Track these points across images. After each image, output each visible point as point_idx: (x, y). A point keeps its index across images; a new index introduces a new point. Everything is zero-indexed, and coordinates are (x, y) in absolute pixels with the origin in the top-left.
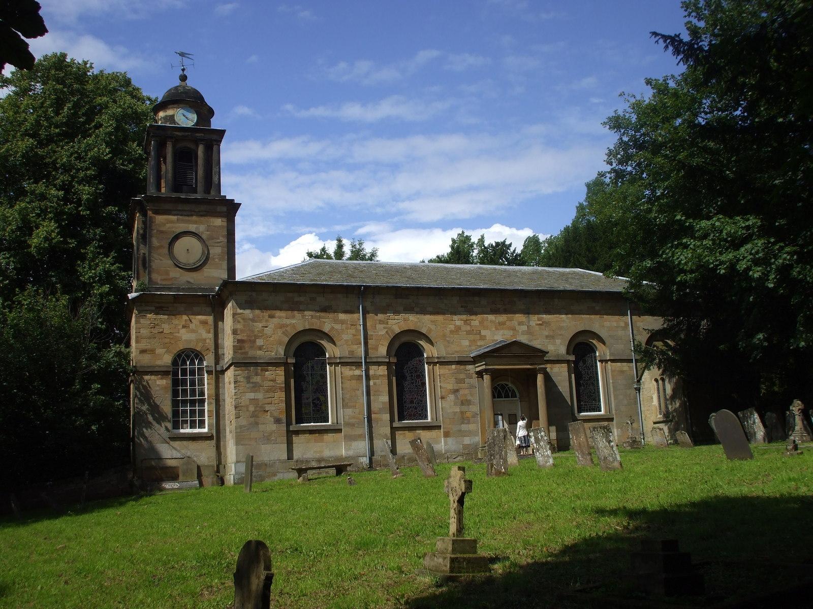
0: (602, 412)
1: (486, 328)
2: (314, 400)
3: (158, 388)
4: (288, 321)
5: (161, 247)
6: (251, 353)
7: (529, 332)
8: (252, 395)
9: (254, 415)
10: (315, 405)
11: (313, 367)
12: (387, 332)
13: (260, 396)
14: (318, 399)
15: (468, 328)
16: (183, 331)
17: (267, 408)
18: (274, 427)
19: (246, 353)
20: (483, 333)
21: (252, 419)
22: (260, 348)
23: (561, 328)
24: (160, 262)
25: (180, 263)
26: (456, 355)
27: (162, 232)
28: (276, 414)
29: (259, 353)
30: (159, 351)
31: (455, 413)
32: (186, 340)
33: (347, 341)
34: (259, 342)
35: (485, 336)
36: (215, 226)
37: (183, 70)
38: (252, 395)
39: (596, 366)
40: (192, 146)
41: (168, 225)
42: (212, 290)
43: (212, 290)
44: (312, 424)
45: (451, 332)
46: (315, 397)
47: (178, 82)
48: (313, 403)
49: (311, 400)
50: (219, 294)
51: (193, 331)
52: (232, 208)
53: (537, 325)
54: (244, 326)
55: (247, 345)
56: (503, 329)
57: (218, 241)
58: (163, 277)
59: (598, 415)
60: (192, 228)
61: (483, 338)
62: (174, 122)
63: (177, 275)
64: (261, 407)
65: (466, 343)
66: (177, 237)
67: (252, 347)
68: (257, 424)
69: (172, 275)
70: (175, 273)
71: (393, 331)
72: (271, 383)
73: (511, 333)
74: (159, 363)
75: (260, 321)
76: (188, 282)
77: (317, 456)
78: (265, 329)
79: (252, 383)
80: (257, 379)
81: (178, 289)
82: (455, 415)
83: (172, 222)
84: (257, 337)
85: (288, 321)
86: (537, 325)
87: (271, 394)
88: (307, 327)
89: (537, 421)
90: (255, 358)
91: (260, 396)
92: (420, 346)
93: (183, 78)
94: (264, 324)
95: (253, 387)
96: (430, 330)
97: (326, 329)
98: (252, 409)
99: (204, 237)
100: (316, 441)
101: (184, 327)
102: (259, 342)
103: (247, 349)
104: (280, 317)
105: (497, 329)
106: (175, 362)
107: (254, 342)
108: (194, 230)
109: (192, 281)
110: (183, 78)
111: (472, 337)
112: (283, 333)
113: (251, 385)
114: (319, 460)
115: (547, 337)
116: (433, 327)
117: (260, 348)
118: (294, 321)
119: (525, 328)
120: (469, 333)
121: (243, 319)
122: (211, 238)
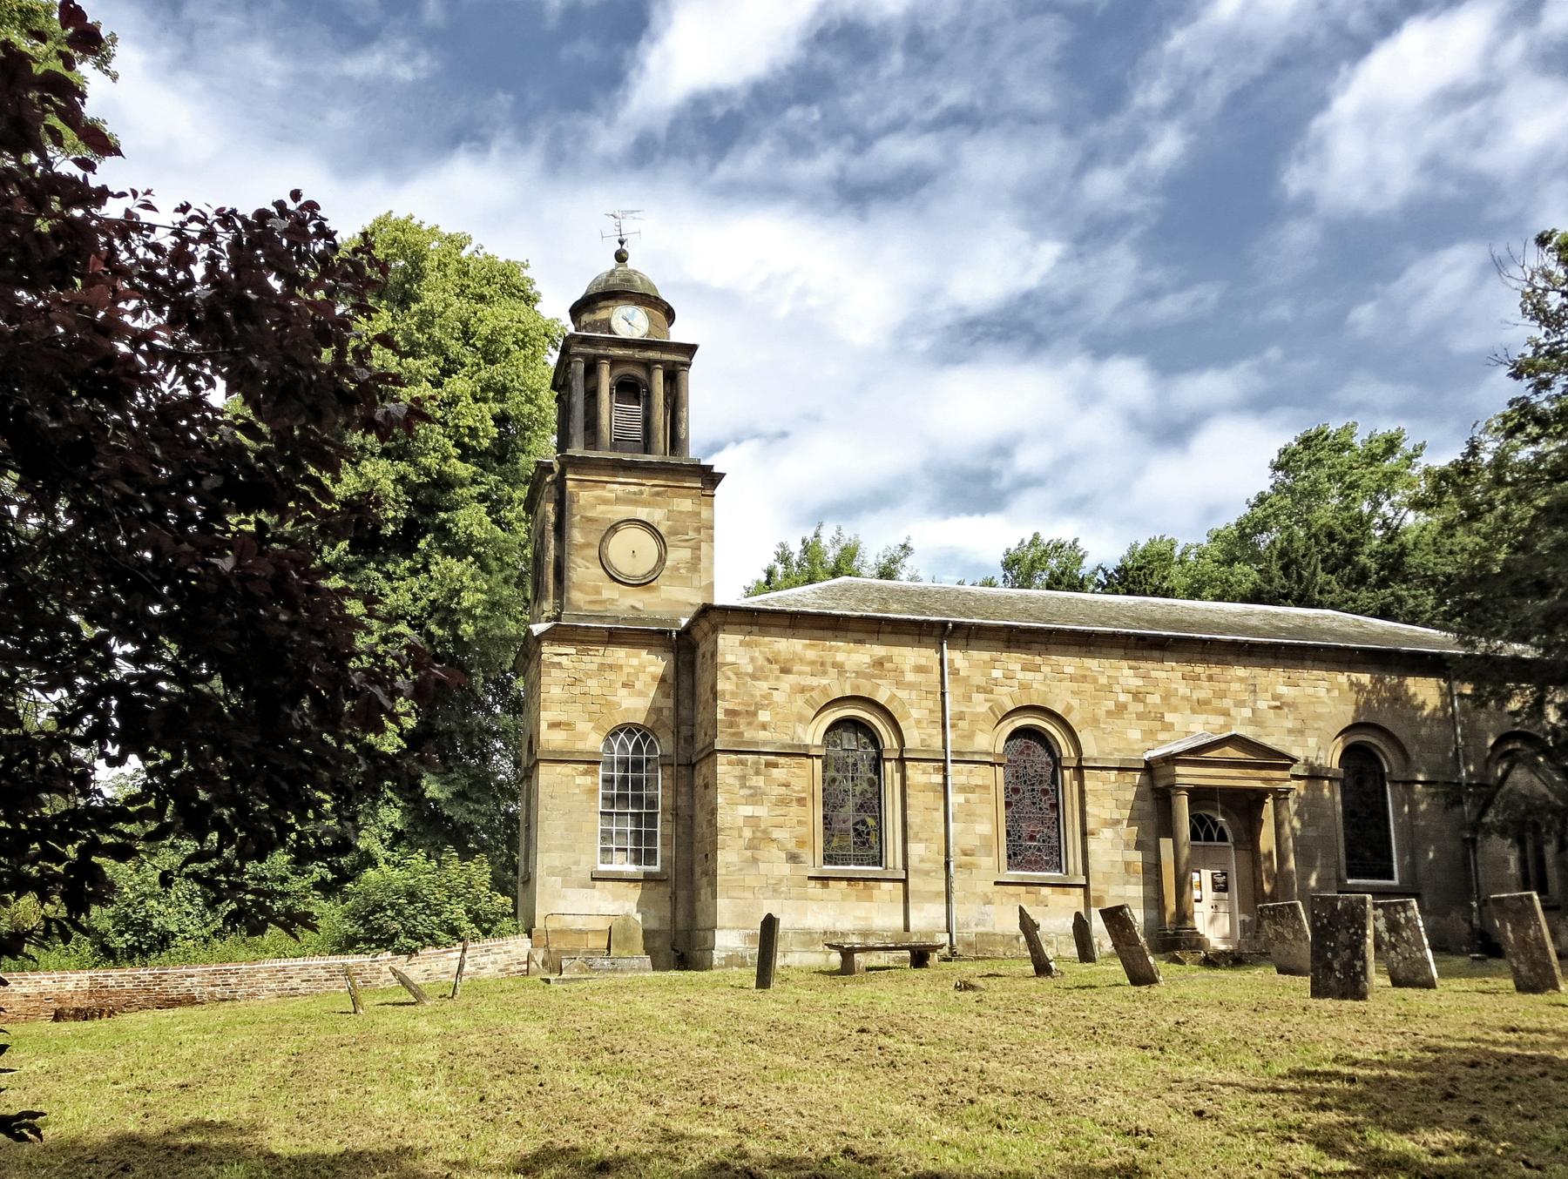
0: (1396, 882)
1: (1175, 709)
2: (857, 823)
3: (577, 791)
4: (815, 681)
5: (588, 545)
6: (748, 735)
7: (1255, 720)
8: (748, 810)
9: (752, 846)
10: (859, 834)
11: (855, 765)
12: (991, 708)
13: (761, 811)
14: (864, 823)
15: (1140, 707)
16: (623, 692)
17: (776, 834)
18: (786, 868)
19: (742, 734)
20: (1169, 717)
21: (749, 853)
22: (764, 727)
23: (1318, 717)
24: (583, 571)
25: (620, 574)
26: (1117, 756)
27: (589, 520)
28: (792, 846)
29: (763, 735)
30: (583, 726)
31: (1113, 863)
32: (627, 710)
33: (918, 722)
34: (764, 716)
35: (1172, 724)
36: (681, 512)
37: (621, 242)
38: (748, 810)
39: (1384, 794)
40: (640, 373)
41: (601, 508)
42: (675, 622)
43: (675, 622)
44: (852, 867)
45: (1109, 713)
46: (858, 819)
47: (612, 263)
48: (855, 830)
49: (850, 824)
50: (687, 631)
51: (641, 694)
52: (710, 478)
53: (1271, 708)
54: (737, 686)
55: (742, 721)
56: (1205, 712)
57: (687, 537)
58: (589, 598)
59: (1388, 886)
60: (642, 513)
61: (1169, 727)
62: (611, 331)
63: (615, 595)
64: (764, 832)
65: (1135, 734)
66: (614, 528)
67: (749, 724)
68: (755, 860)
69: (606, 594)
70: (611, 591)
71: (1001, 706)
72: (783, 790)
73: (1221, 720)
74: (580, 746)
75: (766, 679)
76: (633, 607)
77: (861, 925)
78: (775, 692)
79: (750, 788)
80: (758, 781)
81: (616, 619)
82: (1113, 866)
83: (605, 502)
84: (759, 706)
85: (815, 681)
86: (1271, 708)
87: (783, 810)
88: (848, 693)
89: (646, 926)
90: (756, 743)
91: (761, 811)
92: (1049, 738)
93: (621, 257)
94: (772, 683)
95: (751, 795)
96: (1069, 709)
97: (881, 698)
98: (747, 833)
99: (662, 530)
100: (859, 899)
101: (624, 685)
102: (764, 716)
103: (742, 728)
104: (800, 673)
105: (1194, 712)
106: (609, 746)
107: (755, 714)
108: (644, 519)
109: (640, 606)
110: (621, 257)
111: (1146, 724)
112: (807, 702)
113: (748, 792)
114: (865, 934)
115: (1290, 731)
116: (1075, 702)
117: (764, 727)
118: (824, 681)
119: (1247, 712)
120: (1140, 716)
121: (736, 674)
122: (674, 532)
